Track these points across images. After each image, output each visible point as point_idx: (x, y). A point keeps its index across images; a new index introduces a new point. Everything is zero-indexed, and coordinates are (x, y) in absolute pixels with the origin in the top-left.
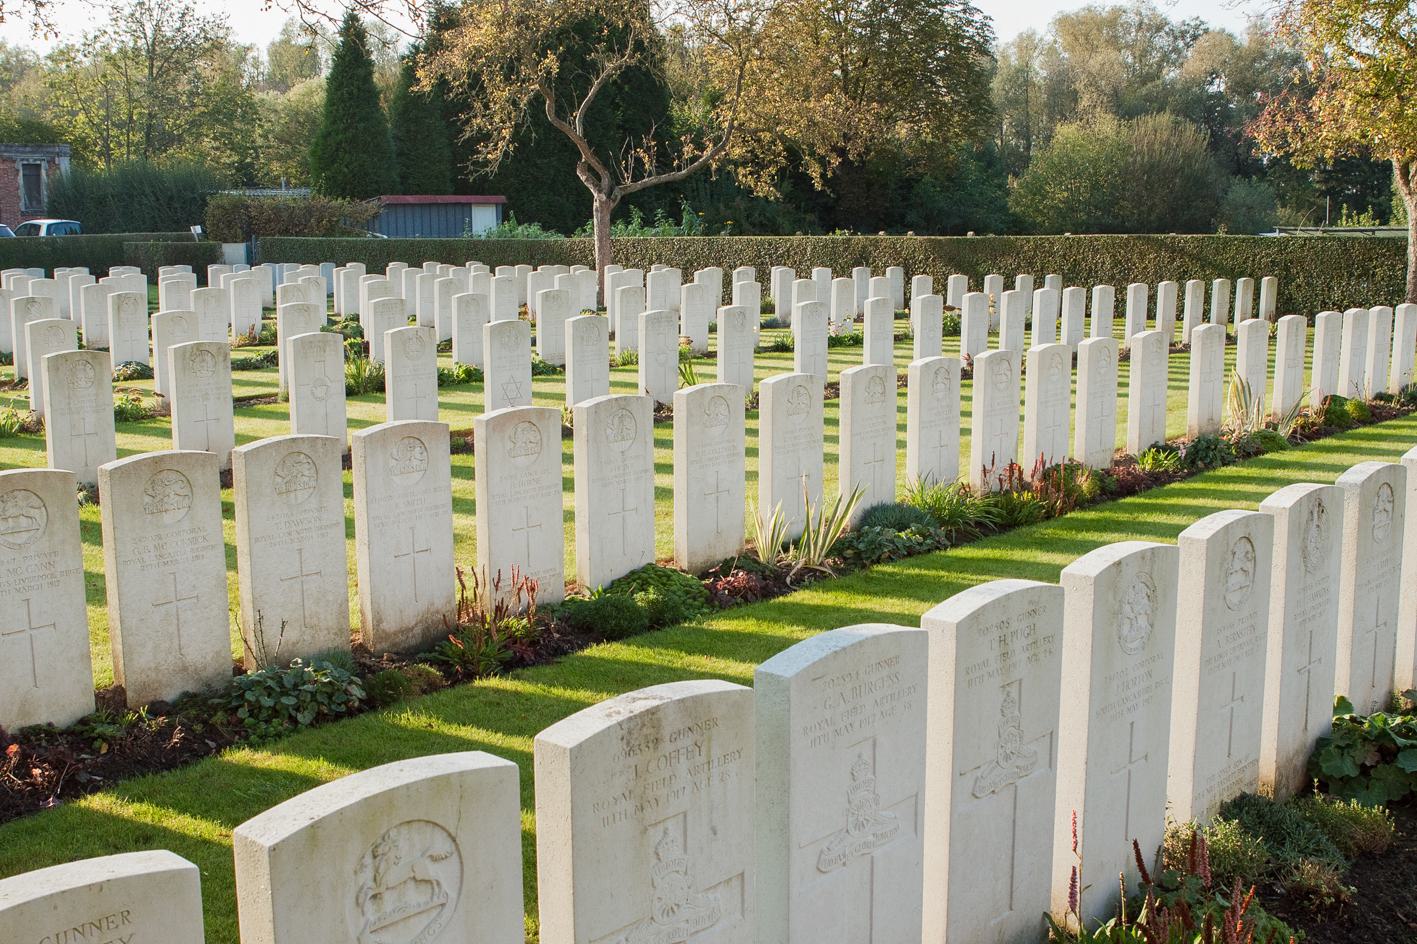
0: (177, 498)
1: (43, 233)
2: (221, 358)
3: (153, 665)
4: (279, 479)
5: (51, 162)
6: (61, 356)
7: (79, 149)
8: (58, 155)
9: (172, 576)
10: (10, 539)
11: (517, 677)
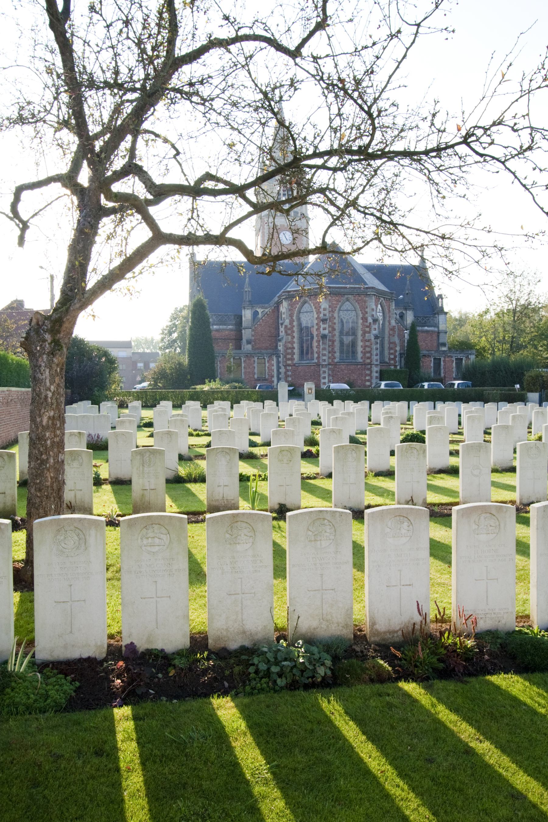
0: (245, 537)
1: (456, 387)
2: (422, 452)
3: (225, 628)
4: (310, 533)
5: (467, 357)
6: (341, 446)
7: (480, 353)
8: (470, 354)
9: (240, 580)
10: (149, 548)
11: (429, 688)
